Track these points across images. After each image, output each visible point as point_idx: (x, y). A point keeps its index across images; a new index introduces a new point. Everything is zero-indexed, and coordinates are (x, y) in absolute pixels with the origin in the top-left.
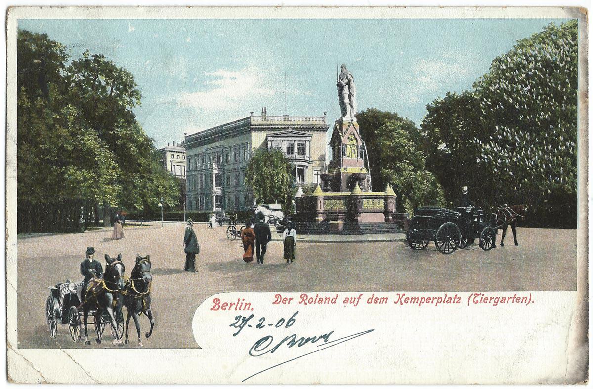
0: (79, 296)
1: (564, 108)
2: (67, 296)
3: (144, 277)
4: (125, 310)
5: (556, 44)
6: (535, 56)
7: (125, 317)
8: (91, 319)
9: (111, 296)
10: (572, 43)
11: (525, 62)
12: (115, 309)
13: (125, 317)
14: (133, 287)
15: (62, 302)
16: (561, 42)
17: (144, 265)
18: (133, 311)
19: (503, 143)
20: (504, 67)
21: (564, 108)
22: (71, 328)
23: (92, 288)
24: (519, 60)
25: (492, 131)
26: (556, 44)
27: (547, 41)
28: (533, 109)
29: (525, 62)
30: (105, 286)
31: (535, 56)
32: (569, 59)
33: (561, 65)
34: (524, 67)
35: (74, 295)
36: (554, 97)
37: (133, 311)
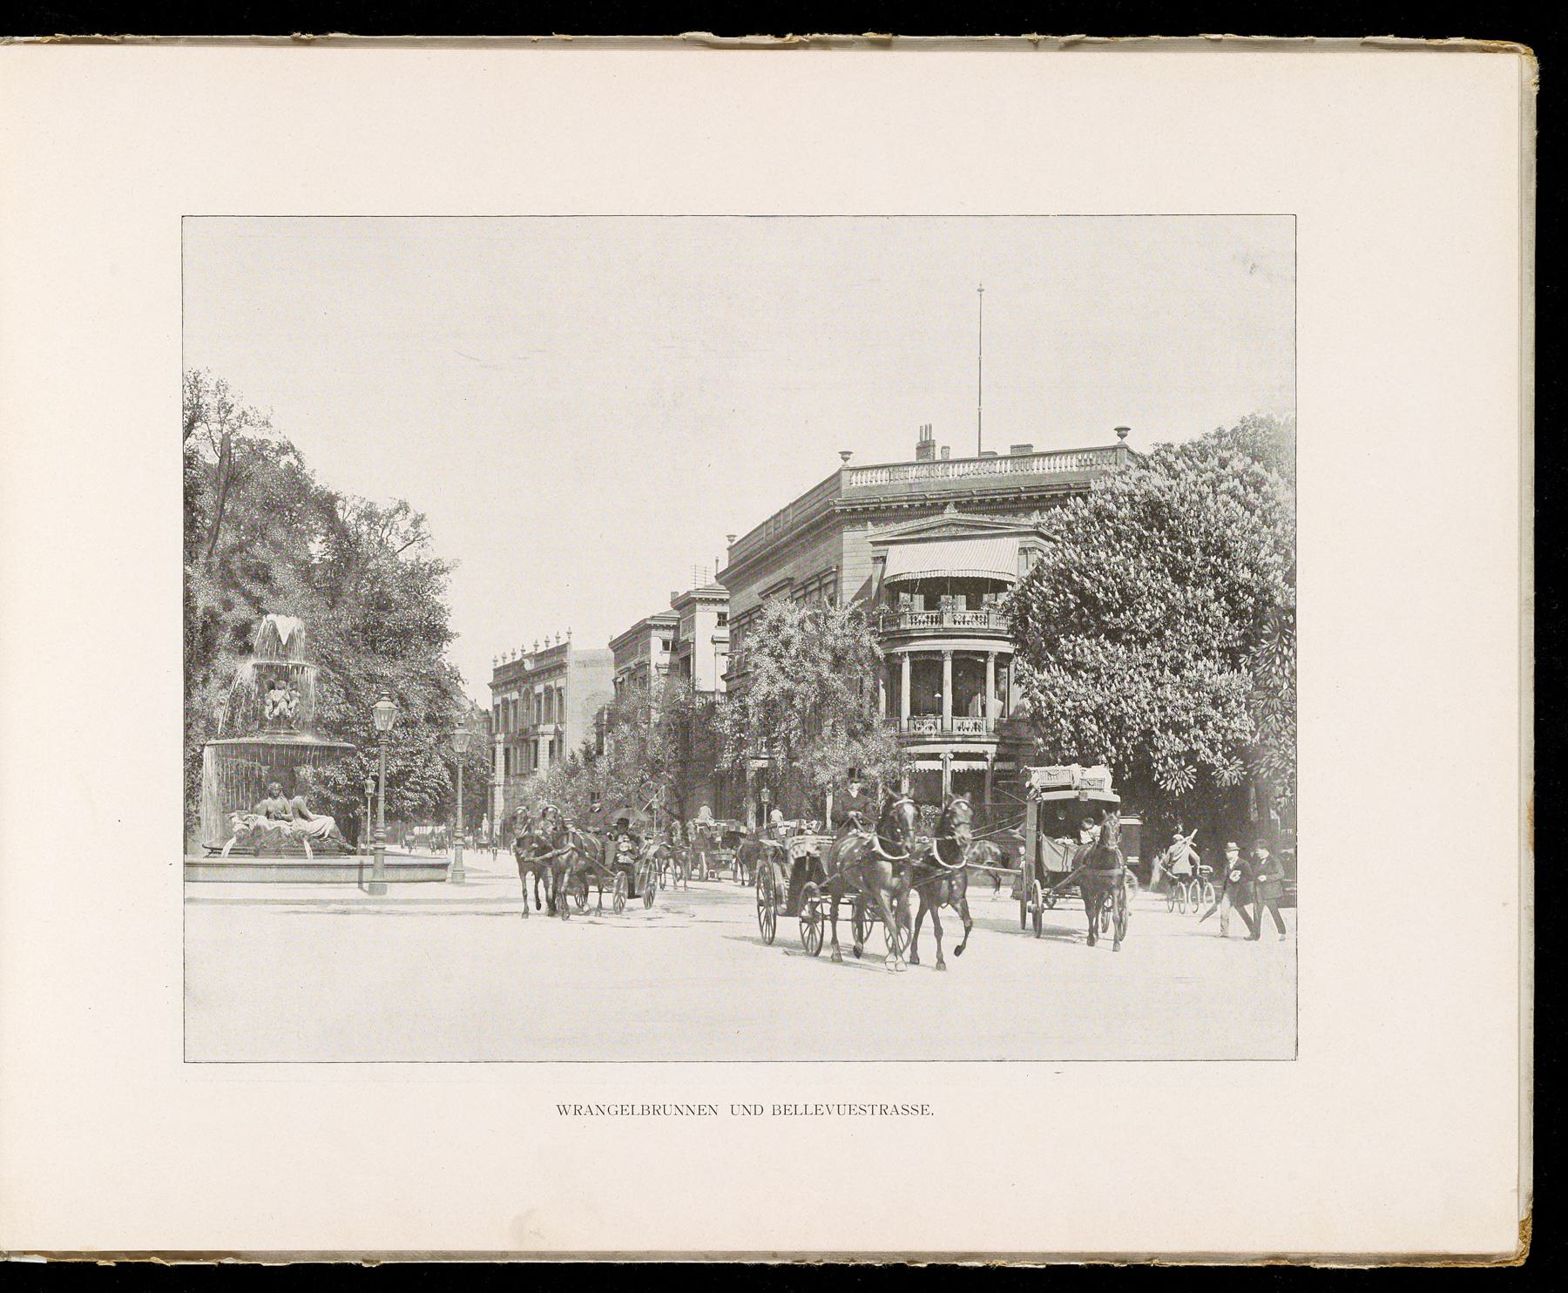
0: (824, 862)
1: (1190, 595)
2: (800, 862)
3: (957, 835)
4: (914, 901)
5: (1169, 467)
6: (1131, 496)
7: (914, 910)
8: (845, 911)
9: (888, 867)
10: (1202, 466)
11: (1111, 506)
12: (896, 893)
13: (914, 910)
14: (935, 853)
15: (789, 873)
16: (1179, 466)
17: (958, 811)
18: (931, 900)
19: (1074, 668)
20: (1072, 518)
21: (1190, 595)
22: (805, 925)
23: (851, 850)
24: (1100, 502)
25: (1053, 645)
26: (1169, 467)
27: (1152, 463)
28: (1129, 599)
29: (1111, 506)
30: (878, 848)
31: (1131, 496)
32: (1195, 497)
33: (1182, 509)
34: (1111, 517)
35: (814, 860)
36: (1172, 573)
37: (931, 900)
